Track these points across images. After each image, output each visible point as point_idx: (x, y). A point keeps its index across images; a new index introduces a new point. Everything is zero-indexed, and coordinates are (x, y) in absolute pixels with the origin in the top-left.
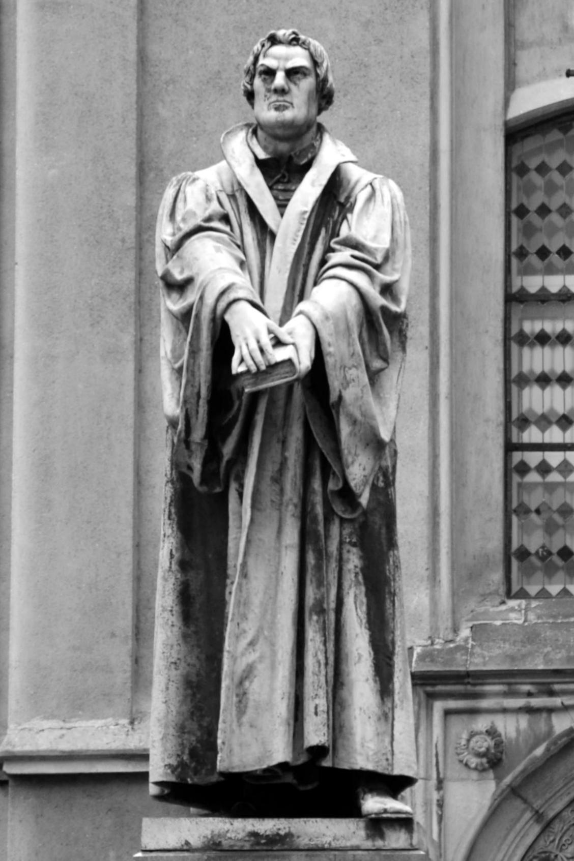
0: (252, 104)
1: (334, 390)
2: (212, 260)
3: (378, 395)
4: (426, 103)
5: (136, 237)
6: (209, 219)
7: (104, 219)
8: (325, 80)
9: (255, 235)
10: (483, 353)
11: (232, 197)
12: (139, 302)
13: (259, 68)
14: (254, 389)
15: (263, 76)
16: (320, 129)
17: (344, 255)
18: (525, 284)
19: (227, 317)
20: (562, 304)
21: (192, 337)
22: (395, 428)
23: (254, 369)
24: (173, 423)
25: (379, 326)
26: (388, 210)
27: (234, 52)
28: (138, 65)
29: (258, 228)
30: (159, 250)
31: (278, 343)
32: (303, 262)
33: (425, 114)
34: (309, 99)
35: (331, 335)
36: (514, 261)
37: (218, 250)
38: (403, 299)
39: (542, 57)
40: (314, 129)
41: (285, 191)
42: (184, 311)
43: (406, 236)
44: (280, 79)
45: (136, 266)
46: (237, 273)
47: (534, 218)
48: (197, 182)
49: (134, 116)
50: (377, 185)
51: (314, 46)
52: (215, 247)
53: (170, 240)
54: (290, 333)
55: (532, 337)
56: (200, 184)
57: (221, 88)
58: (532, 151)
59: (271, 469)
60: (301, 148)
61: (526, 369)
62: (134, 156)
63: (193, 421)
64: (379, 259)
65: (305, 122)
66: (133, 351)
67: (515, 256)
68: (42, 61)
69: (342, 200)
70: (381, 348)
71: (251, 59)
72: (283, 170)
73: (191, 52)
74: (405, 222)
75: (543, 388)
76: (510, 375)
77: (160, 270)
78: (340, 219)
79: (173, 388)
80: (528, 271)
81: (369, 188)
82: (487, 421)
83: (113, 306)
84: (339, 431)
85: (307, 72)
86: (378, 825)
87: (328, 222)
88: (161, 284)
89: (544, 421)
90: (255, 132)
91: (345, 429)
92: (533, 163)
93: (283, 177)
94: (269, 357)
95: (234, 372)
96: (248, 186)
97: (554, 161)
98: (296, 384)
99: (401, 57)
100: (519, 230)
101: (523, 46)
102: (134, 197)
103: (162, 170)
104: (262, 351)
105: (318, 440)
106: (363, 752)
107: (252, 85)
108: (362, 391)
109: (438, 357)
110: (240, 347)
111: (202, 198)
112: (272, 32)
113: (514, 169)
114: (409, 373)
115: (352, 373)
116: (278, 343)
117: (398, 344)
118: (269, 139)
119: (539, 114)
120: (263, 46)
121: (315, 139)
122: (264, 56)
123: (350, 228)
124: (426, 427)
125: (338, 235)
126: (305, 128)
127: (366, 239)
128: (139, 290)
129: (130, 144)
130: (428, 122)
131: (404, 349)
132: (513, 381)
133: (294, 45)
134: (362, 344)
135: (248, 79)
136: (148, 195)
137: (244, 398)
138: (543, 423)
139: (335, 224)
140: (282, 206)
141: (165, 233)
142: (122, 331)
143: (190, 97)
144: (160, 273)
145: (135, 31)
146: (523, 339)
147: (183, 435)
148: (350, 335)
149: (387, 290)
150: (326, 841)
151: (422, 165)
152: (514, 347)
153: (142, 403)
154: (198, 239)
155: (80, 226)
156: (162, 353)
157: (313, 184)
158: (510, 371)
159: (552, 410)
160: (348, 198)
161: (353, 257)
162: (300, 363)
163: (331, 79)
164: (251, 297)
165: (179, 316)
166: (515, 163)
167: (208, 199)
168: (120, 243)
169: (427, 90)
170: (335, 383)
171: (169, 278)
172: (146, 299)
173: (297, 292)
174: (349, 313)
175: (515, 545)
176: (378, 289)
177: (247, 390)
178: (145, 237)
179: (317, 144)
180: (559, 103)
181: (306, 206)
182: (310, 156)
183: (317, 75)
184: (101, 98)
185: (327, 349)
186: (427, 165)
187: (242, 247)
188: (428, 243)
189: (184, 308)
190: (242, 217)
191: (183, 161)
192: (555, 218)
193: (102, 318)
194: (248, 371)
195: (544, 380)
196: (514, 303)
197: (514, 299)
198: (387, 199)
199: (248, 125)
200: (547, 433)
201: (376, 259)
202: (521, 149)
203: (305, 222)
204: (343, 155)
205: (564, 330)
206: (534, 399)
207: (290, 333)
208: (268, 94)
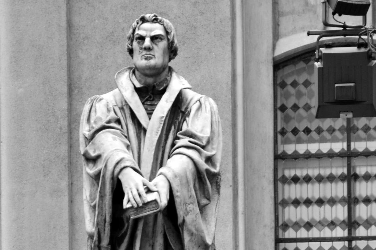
0: (132, 56)
1: (181, 216)
2: (111, 145)
3: (204, 219)
4: (229, 48)
5: (68, 126)
6: (109, 122)
7: (50, 116)
8: (173, 42)
9: (135, 130)
10: (262, 188)
11: (122, 109)
12: (70, 163)
13: (136, 36)
14: (136, 217)
15: (138, 40)
16: (170, 70)
17: (185, 141)
18: (285, 149)
19: (120, 177)
20: (306, 160)
21: (101, 188)
22: (214, 237)
23: (135, 206)
24: (91, 236)
25: (205, 180)
26: (209, 115)
27: (121, 21)
28: (67, 29)
29: (137, 127)
30: (82, 140)
31: (149, 191)
32: (162, 145)
33: (229, 54)
34: (164, 53)
35: (178, 186)
36: (279, 136)
37: (114, 139)
38: (218, 165)
39: (293, 21)
40: (167, 70)
41: (151, 105)
42: (96, 174)
43: (219, 129)
44: (147, 42)
45: (68, 142)
46: (125, 152)
47: (290, 112)
48: (102, 101)
49: (66, 58)
50: (202, 101)
51: (166, 23)
52: (113, 137)
53: (88, 134)
54: (155, 185)
55: (290, 179)
56: (104, 102)
57: (114, 42)
58: (288, 74)
60: (160, 81)
61: (286, 197)
62: (66, 81)
63: (102, 235)
64: (204, 143)
65: (162, 66)
66: (68, 191)
67: (280, 133)
68: (13, 28)
69: (183, 110)
70: (206, 193)
71: (131, 31)
72: (150, 93)
73: (96, 21)
74: (219, 122)
75: (296, 207)
76: (278, 200)
77: (82, 150)
78: (182, 121)
79: (91, 217)
80: (287, 142)
81: (198, 103)
82: (265, 226)
83: (56, 165)
84: (183, 239)
85: (163, 38)
87: (176, 122)
88: (83, 158)
89: (297, 226)
90: (134, 72)
91: (187, 238)
92: (289, 81)
93: (150, 97)
94: (144, 199)
95: (124, 207)
96: (130, 103)
97: (301, 80)
98: (159, 214)
99: (215, 22)
100: (282, 118)
101: (283, 14)
102: (67, 104)
103: (82, 89)
104: (140, 195)
105: (172, 244)
107: (132, 45)
108: (196, 216)
109: (237, 191)
110: (128, 193)
111: (105, 110)
112: (143, 15)
113: (278, 85)
114: (222, 205)
115: (190, 207)
116: (149, 191)
117: (215, 190)
118: (142, 76)
119: (292, 53)
120: (138, 23)
121: (167, 75)
122: (139, 29)
123: (188, 125)
124: (231, 230)
125: (181, 130)
126: (162, 70)
127: (196, 131)
128: (70, 156)
129: (64, 74)
130: (230, 59)
131: (219, 193)
132: (279, 204)
133: (155, 23)
134: (195, 191)
135: (129, 42)
136: (74, 103)
137: (130, 222)
138: (297, 227)
139: (179, 123)
140: (150, 114)
141: (85, 130)
142: (61, 179)
143: (96, 46)
144: (82, 153)
145: (65, 9)
146: (285, 180)
147: (97, 243)
148: (189, 186)
149: (209, 160)
151: (227, 83)
152: (280, 185)
153: (73, 220)
154: (103, 133)
155: (37, 120)
156: (84, 197)
157: (167, 101)
158: (278, 198)
159: (301, 219)
160: (187, 108)
161: (190, 141)
162: (161, 202)
163: (176, 41)
164: (133, 166)
165: (94, 177)
166: (279, 81)
167: (109, 111)
168: (59, 130)
169: (230, 40)
170: (181, 213)
171: (88, 156)
172: (74, 161)
173: (159, 162)
174: (188, 173)
176: (204, 159)
177: (132, 217)
178: (73, 126)
179: (168, 78)
180: (303, 46)
181: (163, 114)
182: (165, 85)
183: (168, 40)
184: (47, 48)
185: (176, 194)
186: (230, 83)
187: (128, 137)
188: (231, 127)
189: (96, 172)
190: (127, 120)
191: (94, 82)
192: (302, 112)
193: (50, 172)
194: (132, 207)
195: (296, 203)
196: (279, 160)
197: (279, 157)
198: (208, 108)
199: (130, 68)
200: (299, 232)
201: (202, 143)
202: (281, 73)
203: (163, 122)
204: (184, 85)
205: (307, 175)
206: (291, 214)
207: (155, 185)
208: (141, 50)
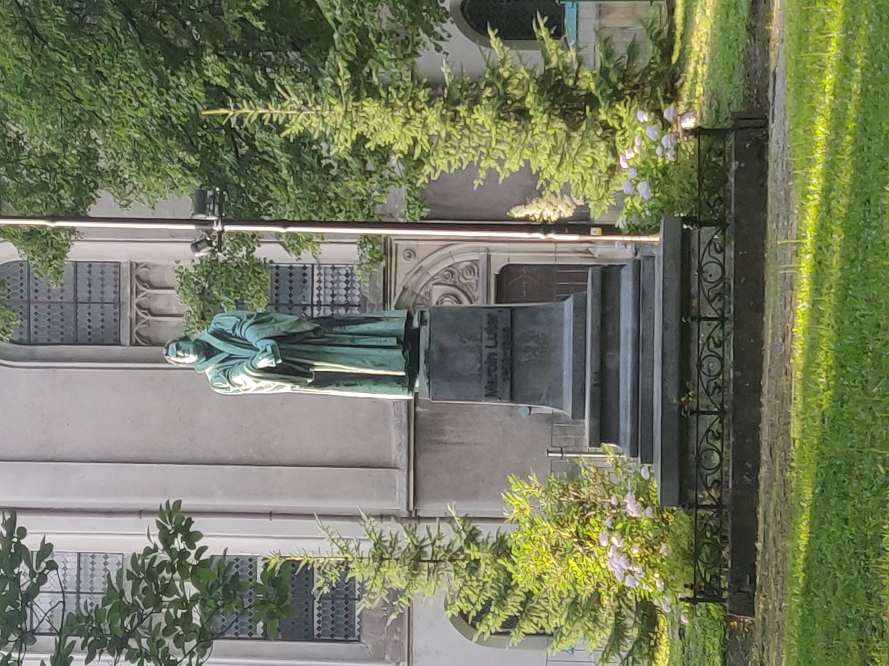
17: (237, 331)
31: (265, 351)
59: (306, 355)
86: (422, 322)
106: (399, 326)
116: (265, 351)
140: (221, 352)
150: (427, 339)
170: (279, 333)
175: (343, 638)
187: (234, 365)
